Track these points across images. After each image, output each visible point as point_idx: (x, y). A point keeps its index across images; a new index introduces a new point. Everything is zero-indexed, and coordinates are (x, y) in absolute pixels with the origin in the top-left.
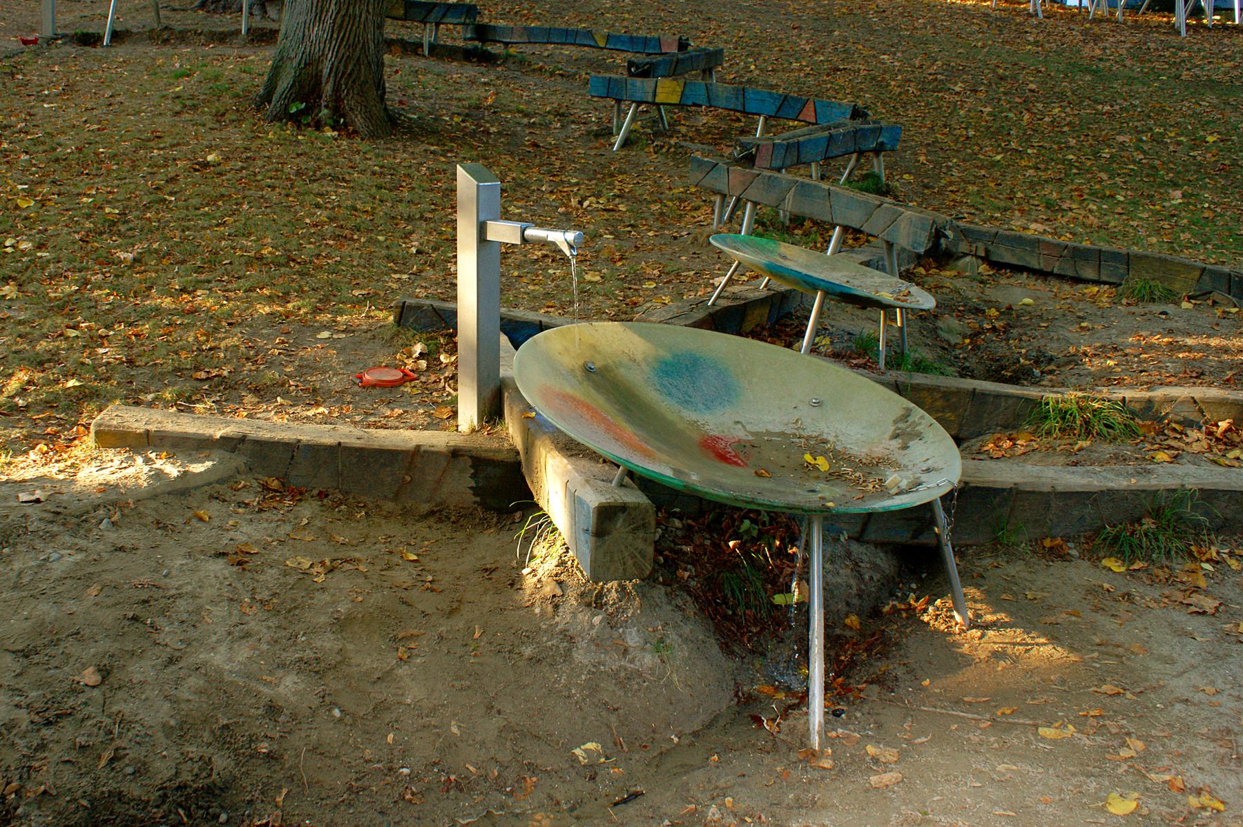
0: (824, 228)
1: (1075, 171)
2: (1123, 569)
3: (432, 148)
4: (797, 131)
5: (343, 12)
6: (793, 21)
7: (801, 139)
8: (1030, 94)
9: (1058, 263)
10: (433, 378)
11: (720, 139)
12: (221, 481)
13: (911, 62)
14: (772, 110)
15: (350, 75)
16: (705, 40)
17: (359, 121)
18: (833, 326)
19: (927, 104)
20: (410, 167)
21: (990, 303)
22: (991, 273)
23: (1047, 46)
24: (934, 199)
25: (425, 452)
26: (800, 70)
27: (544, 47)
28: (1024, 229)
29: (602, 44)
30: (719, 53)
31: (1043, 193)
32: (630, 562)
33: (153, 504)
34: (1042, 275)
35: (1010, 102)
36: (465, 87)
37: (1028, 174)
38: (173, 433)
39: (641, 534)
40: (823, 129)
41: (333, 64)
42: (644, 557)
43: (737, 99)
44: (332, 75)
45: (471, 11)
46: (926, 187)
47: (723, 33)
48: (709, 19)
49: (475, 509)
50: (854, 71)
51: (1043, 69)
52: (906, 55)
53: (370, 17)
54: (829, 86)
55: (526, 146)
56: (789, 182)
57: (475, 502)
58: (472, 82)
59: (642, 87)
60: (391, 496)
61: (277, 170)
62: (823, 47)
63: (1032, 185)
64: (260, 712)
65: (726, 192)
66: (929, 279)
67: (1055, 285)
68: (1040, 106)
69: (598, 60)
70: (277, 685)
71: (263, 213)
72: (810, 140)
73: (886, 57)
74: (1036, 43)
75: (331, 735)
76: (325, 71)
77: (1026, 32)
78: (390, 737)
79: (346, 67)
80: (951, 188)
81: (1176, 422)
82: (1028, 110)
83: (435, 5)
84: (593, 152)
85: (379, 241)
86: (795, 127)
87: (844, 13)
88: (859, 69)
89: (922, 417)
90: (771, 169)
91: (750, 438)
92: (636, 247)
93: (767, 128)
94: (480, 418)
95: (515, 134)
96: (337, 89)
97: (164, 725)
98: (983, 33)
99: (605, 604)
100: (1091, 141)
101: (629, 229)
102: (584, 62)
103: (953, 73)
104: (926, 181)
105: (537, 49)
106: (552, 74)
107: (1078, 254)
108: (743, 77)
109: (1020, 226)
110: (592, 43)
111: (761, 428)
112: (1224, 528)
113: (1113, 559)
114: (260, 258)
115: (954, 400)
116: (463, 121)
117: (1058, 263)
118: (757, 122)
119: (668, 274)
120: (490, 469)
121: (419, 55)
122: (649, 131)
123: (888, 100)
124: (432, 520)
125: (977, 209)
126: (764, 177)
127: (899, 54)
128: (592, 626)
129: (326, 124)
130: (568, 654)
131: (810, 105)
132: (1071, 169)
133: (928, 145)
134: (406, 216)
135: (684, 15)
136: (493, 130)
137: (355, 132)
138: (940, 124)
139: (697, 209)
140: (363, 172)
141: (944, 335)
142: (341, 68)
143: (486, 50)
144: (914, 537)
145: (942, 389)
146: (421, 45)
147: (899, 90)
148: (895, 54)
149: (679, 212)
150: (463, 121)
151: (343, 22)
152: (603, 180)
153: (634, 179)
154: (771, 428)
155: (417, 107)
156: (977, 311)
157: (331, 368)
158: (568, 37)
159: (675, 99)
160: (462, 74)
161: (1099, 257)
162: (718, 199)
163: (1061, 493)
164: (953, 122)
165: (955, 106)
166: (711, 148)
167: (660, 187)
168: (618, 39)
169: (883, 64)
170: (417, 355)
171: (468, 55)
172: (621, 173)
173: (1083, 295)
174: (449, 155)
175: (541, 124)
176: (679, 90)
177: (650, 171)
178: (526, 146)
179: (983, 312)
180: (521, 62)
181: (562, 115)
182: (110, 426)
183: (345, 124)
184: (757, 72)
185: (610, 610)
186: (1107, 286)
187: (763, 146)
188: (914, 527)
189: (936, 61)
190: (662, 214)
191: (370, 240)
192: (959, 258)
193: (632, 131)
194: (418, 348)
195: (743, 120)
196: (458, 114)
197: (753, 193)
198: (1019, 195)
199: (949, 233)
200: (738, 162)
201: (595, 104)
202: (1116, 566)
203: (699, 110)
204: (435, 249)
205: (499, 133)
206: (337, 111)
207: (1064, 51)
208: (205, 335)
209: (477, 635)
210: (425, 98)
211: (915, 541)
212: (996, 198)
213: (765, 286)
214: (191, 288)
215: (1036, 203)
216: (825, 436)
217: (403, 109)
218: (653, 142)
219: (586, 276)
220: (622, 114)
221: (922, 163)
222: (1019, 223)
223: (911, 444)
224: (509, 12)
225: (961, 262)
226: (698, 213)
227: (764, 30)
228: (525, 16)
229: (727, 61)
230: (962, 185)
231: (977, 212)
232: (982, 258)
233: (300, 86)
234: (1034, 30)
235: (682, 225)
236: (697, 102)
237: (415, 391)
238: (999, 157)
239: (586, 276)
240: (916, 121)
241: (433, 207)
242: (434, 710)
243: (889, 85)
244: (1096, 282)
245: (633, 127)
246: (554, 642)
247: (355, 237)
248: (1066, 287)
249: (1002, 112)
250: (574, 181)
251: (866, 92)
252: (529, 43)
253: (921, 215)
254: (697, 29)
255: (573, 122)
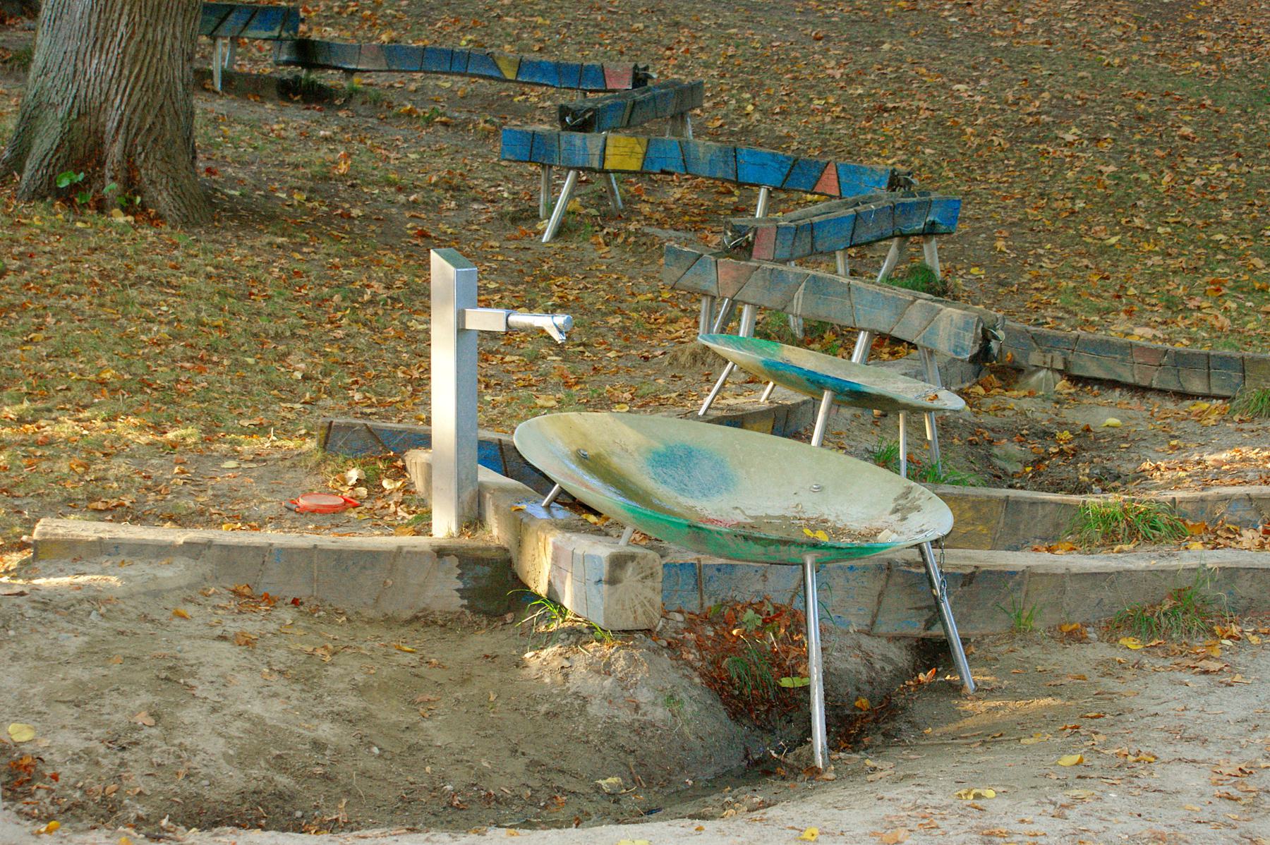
0: (846, 338)
1: (1220, 257)
2: (1140, 647)
3: (280, 240)
4: (814, 209)
5: (137, 38)
6: (815, 25)
7: (816, 219)
8: (1180, 143)
9: (1156, 374)
10: (380, 504)
11: (702, 222)
12: (190, 586)
13: (1002, 95)
14: (777, 179)
15: (150, 129)
16: (673, 62)
17: (163, 200)
18: (852, 447)
19: (1020, 163)
20: (256, 267)
21: (1062, 425)
22: (1073, 390)
23: (1227, 60)
24: (1012, 298)
25: (408, 552)
26: (826, 111)
27: (407, 76)
28: (1127, 334)
29: (510, 75)
30: (696, 88)
31: (1167, 287)
32: (640, 611)
33: (132, 603)
34: (1140, 390)
35: (1147, 157)
36: (297, 146)
37: (1150, 263)
38: (129, 540)
39: (649, 582)
40: (847, 205)
41: (122, 114)
42: (653, 606)
43: (726, 163)
44: (122, 131)
45: (289, 17)
46: (1001, 284)
47: (702, 49)
48: (677, 24)
49: (462, 613)
50: (911, 112)
51: (1208, 102)
52: (995, 83)
53: (177, 45)
54: (869, 136)
55: (409, 236)
56: (798, 276)
57: (462, 606)
58: (305, 136)
59: (587, 145)
60: (371, 602)
61: (72, 272)
62: (862, 72)
63: (1153, 278)
64: (307, 747)
65: (715, 292)
66: (989, 400)
67: (1154, 399)
68: (1192, 161)
69: (501, 98)
70: (316, 730)
71: (80, 328)
72: (828, 221)
73: (962, 87)
74: (1212, 58)
75: (376, 766)
76: (109, 124)
77: (1199, 38)
78: (428, 769)
79: (143, 120)
80: (1036, 285)
81: (1230, 523)
82: (1172, 168)
83: (231, 9)
84: (512, 245)
85: (248, 364)
86: (816, 202)
87: (902, 9)
88: (919, 108)
89: (922, 493)
90: (775, 260)
91: (749, 521)
92: (595, 369)
93: (771, 207)
94: (459, 525)
95: (388, 219)
96: (129, 155)
97: (224, 754)
98: (1128, 40)
99: (614, 672)
100: (1256, 213)
101: (581, 348)
102: (477, 101)
103: (1065, 111)
104: (1002, 276)
105: (397, 80)
106: (429, 122)
107: (1182, 361)
108: (735, 125)
109: (1122, 332)
110: (495, 74)
111: (761, 513)
112: (1246, 610)
113: (1131, 638)
114: (103, 383)
115: (985, 510)
116: (308, 200)
117: (1156, 374)
118: (756, 196)
119: (642, 397)
120: (478, 568)
121: (207, 90)
122: (593, 212)
123: (959, 157)
124: (417, 625)
125: (1068, 312)
126: (764, 271)
127: (984, 82)
128: (603, 688)
129: (113, 206)
130: (582, 709)
131: (831, 171)
132: (1215, 254)
133: (1013, 224)
134: (272, 333)
135: (634, 17)
136: (356, 212)
137: (159, 216)
138: (1034, 192)
139: (673, 321)
140: (193, 273)
141: (998, 462)
142: (136, 120)
143: (314, 82)
144: (927, 628)
145: (971, 499)
146: (211, 74)
147: (977, 141)
148: (977, 81)
149: (649, 326)
150: (308, 200)
151: (138, 51)
152: (534, 284)
153: (578, 282)
154: (770, 512)
155: (235, 178)
156: (1046, 434)
157: (254, 496)
158: (454, 62)
159: (634, 165)
160: (287, 123)
161: (1209, 364)
162: (704, 305)
163: (1076, 574)
164: (1055, 189)
165: (1063, 162)
166: (689, 235)
167: (617, 292)
168: (537, 67)
169: (957, 98)
170: (353, 481)
171: (288, 91)
172: (559, 275)
173: (1189, 413)
174: (305, 250)
175: (426, 203)
176: (640, 150)
177: (601, 271)
178: (409, 236)
179: (1053, 435)
180: (376, 102)
181: (457, 188)
182: (56, 535)
183: (143, 206)
184: (757, 116)
185: (619, 675)
186: (1220, 401)
187: (762, 230)
188: (926, 617)
189: (1043, 91)
190: (625, 329)
191: (236, 363)
192: (1032, 373)
193: (568, 213)
194: (353, 474)
195: (737, 192)
196: (300, 189)
197: (750, 293)
198: (1132, 291)
199: (1001, 334)
200: (727, 252)
201: (506, 171)
202: (1132, 643)
203: (669, 178)
204: (326, 374)
205: (365, 217)
206: (130, 184)
207: (1252, 69)
208: (81, 465)
209: (492, 699)
210: (244, 164)
211: (929, 632)
212: (1098, 296)
213: (767, 399)
214: (30, 418)
215: (1154, 301)
216: (826, 517)
217: (215, 181)
218: (602, 228)
219: (537, 401)
220: (554, 189)
221: (1001, 251)
222: (1122, 328)
223: (909, 516)
224: (339, 13)
225: (1034, 380)
226: (676, 326)
227: (767, 44)
228: (366, 19)
229: (709, 99)
230: (1053, 280)
231: (1067, 316)
232: (1060, 371)
233: (72, 148)
234: (1211, 34)
235: (655, 342)
236: (667, 169)
237: (362, 517)
238: (1113, 240)
239: (537, 401)
240: (998, 189)
241: (304, 321)
242: (464, 750)
243: (963, 132)
244: (1207, 397)
245: (575, 204)
246: (569, 700)
247: (215, 359)
248: (1170, 405)
249: (1131, 173)
250: (493, 286)
251: (926, 146)
252: (389, 71)
253: (966, 312)
254: (658, 42)
255: (475, 200)
